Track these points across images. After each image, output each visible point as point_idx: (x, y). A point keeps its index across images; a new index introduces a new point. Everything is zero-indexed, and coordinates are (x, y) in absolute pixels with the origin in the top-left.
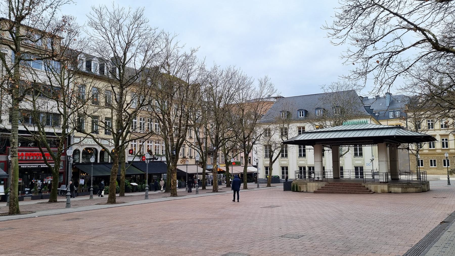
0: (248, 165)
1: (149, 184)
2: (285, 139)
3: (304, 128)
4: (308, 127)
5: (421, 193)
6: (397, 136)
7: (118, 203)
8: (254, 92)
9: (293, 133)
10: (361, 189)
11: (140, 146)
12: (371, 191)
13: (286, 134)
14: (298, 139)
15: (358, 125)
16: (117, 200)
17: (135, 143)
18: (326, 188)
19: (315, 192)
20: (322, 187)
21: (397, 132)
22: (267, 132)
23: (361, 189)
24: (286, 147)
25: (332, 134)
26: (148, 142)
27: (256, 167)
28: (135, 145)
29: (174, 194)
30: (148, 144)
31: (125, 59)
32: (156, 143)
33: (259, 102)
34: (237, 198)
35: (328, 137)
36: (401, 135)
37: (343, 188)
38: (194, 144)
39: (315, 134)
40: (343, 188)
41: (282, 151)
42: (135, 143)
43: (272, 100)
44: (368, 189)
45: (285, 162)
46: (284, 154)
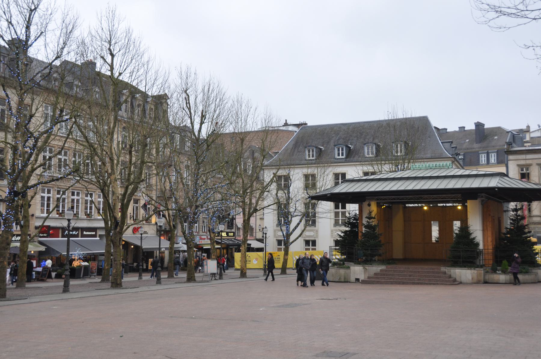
0: (248, 238)
1: (4, 225)
2: (312, 193)
3: (344, 175)
4: (353, 171)
5: (535, 285)
6: (499, 188)
7: (9, 300)
8: (254, 124)
9: (326, 182)
10: (439, 277)
11: (58, 199)
12: (455, 280)
13: (314, 186)
14: (337, 190)
15: (435, 171)
16: (8, 293)
17: (49, 195)
18: (381, 275)
19: (364, 282)
20: (375, 274)
21: (500, 182)
22: (284, 183)
23: (439, 277)
24: (314, 206)
25: (393, 183)
26: (73, 194)
27: (261, 241)
28: (49, 198)
29: (117, 284)
30: (73, 197)
31: (27, 40)
32: (65, 160)
33: (267, 133)
34: (528, 127)
35: (387, 189)
36: (507, 186)
37: (410, 276)
38: (154, 198)
39: (366, 184)
40: (410, 276)
41: (306, 215)
42: (49, 195)
43: (291, 128)
44: (450, 277)
45: (312, 234)
46: (310, 218)
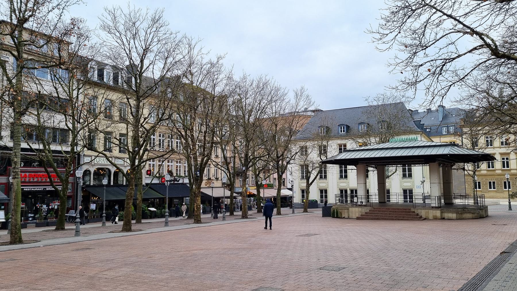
0: (282, 188)
2: (324, 158)
3: (345, 145)
4: (350, 145)
5: (478, 220)
6: (451, 155)
7: (134, 231)
8: (289, 104)
9: (333, 152)
10: (410, 215)
11: (160, 165)
12: (421, 217)
13: (326, 152)
14: (339, 158)
15: (406, 143)
16: (133, 228)
17: (154, 163)
18: (370, 213)
19: (358, 218)
20: (366, 213)
21: (451, 150)
22: (304, 150)
23: (410, 215)
24: (325, 167)
25: (377, 152)
26: (168, 162)
27: (291, 189)
28: (154, 165)
29: (198, 221)
30: (168, 164)
31: (142, 68)
33: (294, 116)
34: (269, 225)
35: (372, 156)
36: (456, 153)
37: (390, 214)
38: (220, 164)
39: (358, 153)
40: (390, 214)
41: (320, 172)
42: (154, 163)
43: (309, 113)
44: (418, 215)
45: (324, 185)
46: (323, 175)
